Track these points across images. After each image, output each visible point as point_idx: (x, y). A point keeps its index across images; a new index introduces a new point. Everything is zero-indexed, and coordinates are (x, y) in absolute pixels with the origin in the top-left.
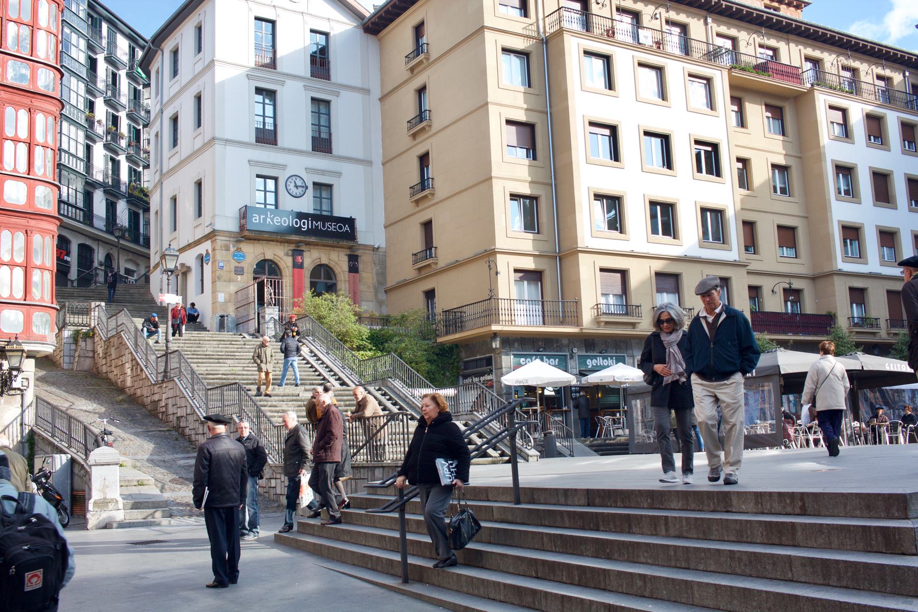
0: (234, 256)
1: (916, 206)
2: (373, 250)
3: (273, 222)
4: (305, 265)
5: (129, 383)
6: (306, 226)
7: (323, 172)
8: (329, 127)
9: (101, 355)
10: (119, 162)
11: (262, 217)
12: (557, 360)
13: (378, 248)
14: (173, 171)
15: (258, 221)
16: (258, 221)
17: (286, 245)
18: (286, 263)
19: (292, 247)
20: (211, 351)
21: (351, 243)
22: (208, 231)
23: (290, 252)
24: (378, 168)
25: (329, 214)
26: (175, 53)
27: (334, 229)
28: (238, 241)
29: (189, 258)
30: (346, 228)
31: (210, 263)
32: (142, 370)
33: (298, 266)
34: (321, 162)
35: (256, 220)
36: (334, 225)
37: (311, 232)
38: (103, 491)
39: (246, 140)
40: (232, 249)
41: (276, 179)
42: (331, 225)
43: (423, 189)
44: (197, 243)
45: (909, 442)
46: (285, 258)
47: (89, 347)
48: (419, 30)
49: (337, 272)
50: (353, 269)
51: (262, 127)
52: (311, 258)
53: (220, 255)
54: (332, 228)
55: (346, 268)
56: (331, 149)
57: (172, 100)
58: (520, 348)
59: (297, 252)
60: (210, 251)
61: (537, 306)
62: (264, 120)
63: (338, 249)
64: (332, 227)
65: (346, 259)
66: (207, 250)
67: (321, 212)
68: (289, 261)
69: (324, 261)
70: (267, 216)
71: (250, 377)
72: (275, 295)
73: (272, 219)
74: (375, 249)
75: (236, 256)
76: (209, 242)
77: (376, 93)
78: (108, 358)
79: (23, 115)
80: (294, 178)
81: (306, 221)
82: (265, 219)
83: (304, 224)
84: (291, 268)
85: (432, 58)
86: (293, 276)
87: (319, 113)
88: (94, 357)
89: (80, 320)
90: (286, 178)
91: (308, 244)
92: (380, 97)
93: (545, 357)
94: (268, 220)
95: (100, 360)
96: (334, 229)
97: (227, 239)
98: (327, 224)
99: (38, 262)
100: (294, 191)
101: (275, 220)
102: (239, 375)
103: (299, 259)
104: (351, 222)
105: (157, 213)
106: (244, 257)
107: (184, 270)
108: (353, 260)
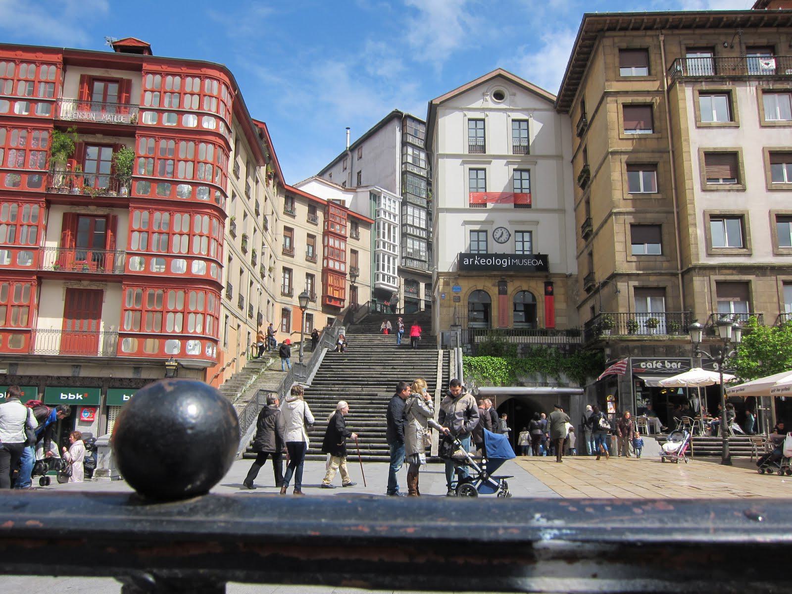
0: (453, 289)
1: (789, 180)
3: (480, 263)
12: (680, 364)
17: (494, 278)
18: (494, 291)
19: (499, 279)
21: (544, 274)
25: (485, 252)
28: (456, 279)
30: (540, 262)
33: (503, 292)
39: (462, 207)
40: (452, 284)
41: (486, 231)
46: (493, 288)
50: (549, 294)
55: (543, 292)
58: (640, 353)
61: (661, 318)
63: (537, 278)
65: (543, 285)
67: (523, 253)
68: (496, 290)
70: (475, 259)
73: (479, 261)
79: (412, 209)
80: (503, 230)
82: (473, 262)
83: (504, 262)
84: (497, 295)
86: (499, 301)
89: (16, 342)
90: (494, 230)
91: (511, 276)
93: (666, 362)
100: (497, 235)
103: (550, 288)
104: (544, 258)
108: (548, 284)
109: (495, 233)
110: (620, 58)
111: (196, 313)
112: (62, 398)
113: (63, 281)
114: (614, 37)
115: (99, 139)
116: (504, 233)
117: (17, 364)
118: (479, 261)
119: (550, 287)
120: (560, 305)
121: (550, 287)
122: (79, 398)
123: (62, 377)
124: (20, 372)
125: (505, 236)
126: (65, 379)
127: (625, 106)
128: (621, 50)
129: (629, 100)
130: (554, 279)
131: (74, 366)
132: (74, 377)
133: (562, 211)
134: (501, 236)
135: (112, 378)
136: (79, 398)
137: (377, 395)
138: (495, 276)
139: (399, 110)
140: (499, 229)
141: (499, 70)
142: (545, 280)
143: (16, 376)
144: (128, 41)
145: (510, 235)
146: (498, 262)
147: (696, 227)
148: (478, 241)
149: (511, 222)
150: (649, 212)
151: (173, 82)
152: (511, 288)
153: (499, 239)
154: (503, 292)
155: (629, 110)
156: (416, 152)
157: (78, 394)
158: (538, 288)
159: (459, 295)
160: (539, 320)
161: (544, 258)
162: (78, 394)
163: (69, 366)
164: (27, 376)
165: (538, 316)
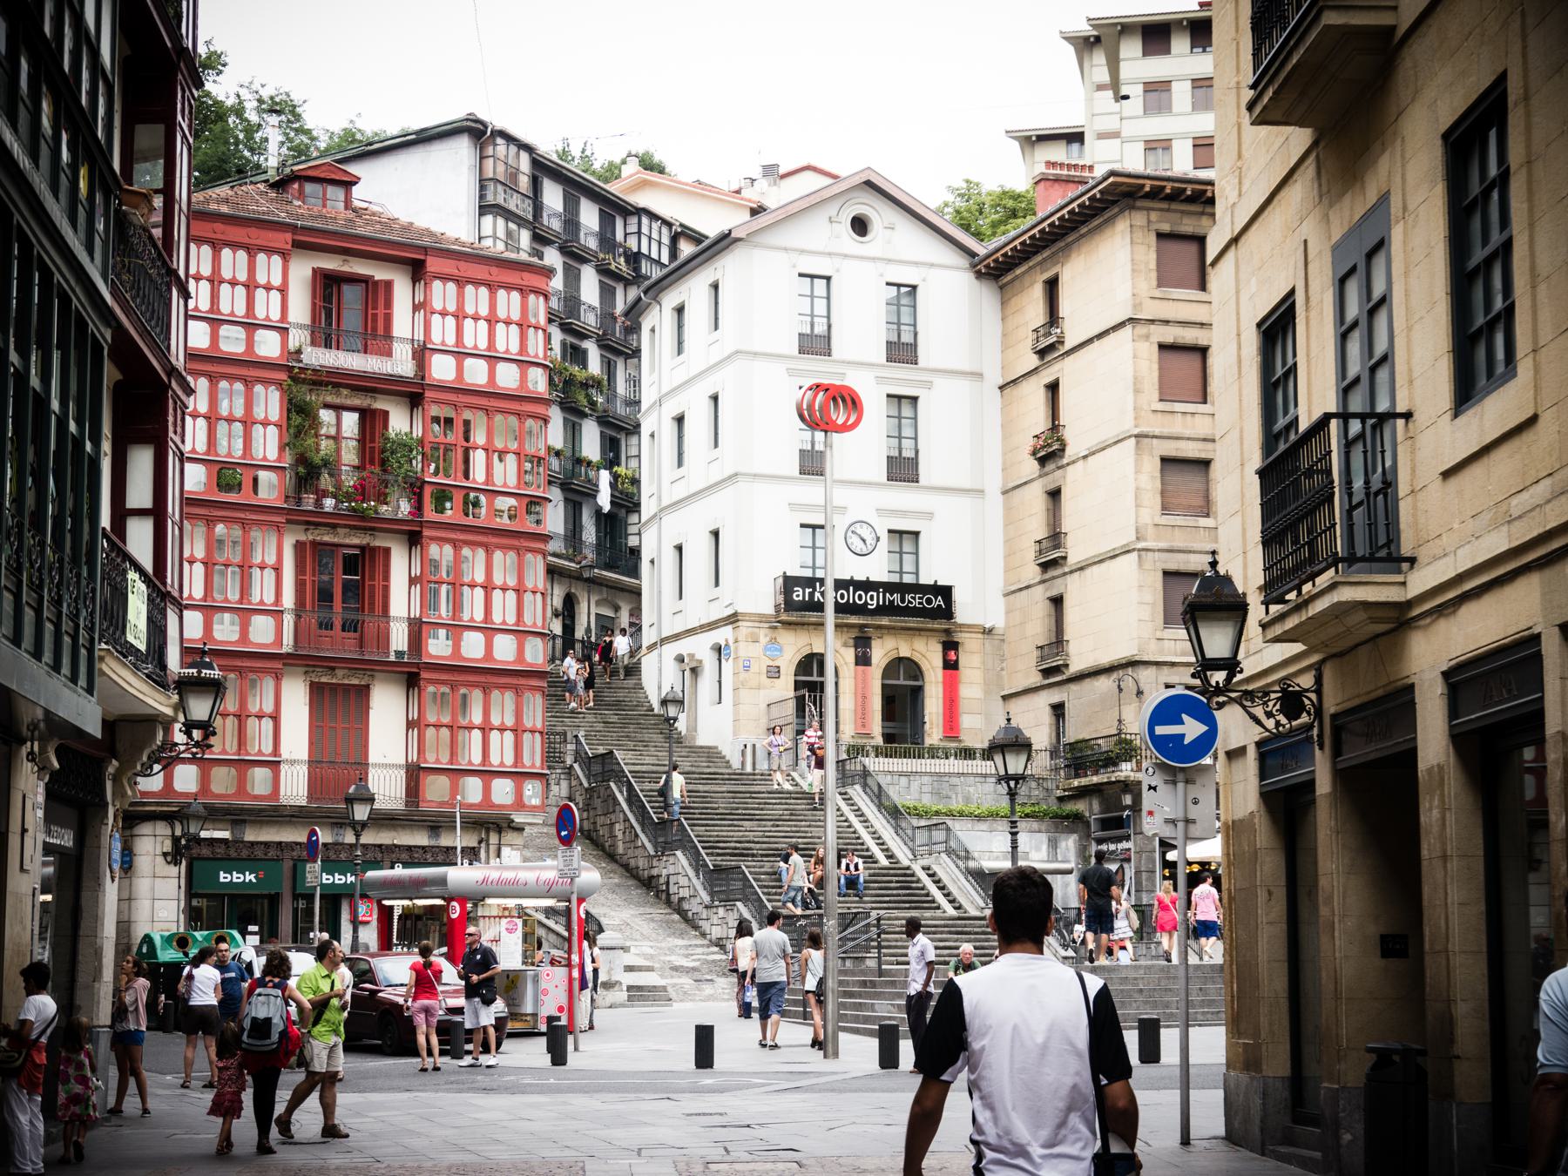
0: (766, 649)
2: (984, 633)
4: (874, 660)
10: (585, 352)
11: (808, 591)
20: (726, 808)
21: (944, 625)
22: (729, 611)
23: (851, 642)
24: (995, 500)
26: (680, 310)
29: (699, 648)
30: (939, 601)
31: (731, 659)
32: (637, 836)
33: (863, 660)
34: (902, 497)
38: (609, 972)
42: (914, 598)
43: (1057, 546)
48: (1052, 285)
49: (924, 668)
50: (951, 666)
51: (809, 448)
53: (746, 650)
54: (916, 603)
60: (731, 642)
64: (915, 601)
65: (939, 648)
70: (815, 590)
74: (988, 632)
75: (770, 649)
78: (592, 813)
82: (812, 595)
97: (757, 624)
98: (908, 597)
99: (528, 724)
100: (858, 545)
102: (758, 843)
104: (946, 592)
105: (652, 435)
106: (781, 650)
108: (950, 646)
110: (1158, 252)
111: (437, 726)
112: (222, 880)
113: (304, 669)
114: (1149, 209)
115: (345, 397)
117: (244, 821)
119: (953, 653)
120: (972, 685)
121: (953, 653)
124: (250, 835)
126: (421, 851)
127: (1163, 347)
128: (1161, 236)
129: (1170, 335)
130: (963, 635)
131: (336, 823)
132: (336, 844)
135: (396, 846)
141: (869, 172)
143: (243, 842)
144: (324, 168)
145: (878, 539)
148: (814, 547)
150: (1194, 552)
151: (476, 298)
152: (881, 652)
154: (863, 660)
155: (1171, 356)
156: (512, 226)
158: (929, 655)
159: (776, 663)
161: (946, 592)
163: (227, 820)
164: (261, 843)
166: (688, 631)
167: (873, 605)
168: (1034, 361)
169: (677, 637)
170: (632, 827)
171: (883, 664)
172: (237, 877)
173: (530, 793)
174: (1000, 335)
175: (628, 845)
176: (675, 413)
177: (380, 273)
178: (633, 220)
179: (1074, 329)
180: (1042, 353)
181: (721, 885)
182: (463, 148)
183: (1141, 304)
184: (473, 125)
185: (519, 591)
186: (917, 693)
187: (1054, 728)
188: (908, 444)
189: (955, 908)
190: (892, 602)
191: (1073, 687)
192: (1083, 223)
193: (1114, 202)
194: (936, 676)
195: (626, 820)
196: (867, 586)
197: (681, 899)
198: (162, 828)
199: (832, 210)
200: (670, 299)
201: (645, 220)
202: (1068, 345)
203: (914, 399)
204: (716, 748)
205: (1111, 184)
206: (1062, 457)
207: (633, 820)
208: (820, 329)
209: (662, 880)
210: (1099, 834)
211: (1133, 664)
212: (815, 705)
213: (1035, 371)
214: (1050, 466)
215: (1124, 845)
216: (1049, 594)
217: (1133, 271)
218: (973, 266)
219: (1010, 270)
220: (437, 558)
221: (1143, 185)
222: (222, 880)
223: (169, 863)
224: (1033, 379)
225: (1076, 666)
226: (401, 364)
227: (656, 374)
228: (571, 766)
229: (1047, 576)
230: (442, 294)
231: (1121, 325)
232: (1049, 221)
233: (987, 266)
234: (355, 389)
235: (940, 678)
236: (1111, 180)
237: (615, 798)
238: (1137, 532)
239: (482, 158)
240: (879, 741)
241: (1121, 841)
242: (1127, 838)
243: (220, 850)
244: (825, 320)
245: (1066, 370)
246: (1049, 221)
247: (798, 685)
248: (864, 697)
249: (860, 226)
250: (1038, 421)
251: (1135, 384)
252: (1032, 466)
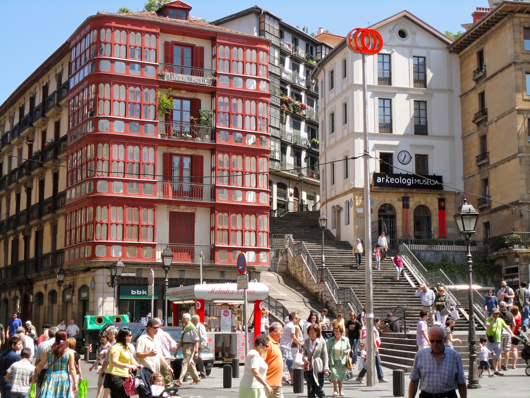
3: (389, 181)
5: (305, 282)
6: (410, 183)
7: (422, 147)
8: (426, 118)
9: (291, 264)
11: (383, 178)
13: (459, 193)
14: (331, 147)
15: (380, 181)
16: (380, 181)
18: (398, 205)
27: (428, 183)
32: (311, 276)
33: (406, 206)
34: (421, 140)
35: (379, 181)
36: (428, 181)
37: (414, 186)
42: (426, 181)
44: (345, 194)
45: (215, 334)
47: (285, 260)
48: (481, 55)
52: (415, 201)
56: (427, 132)
57: (330, 102)
59: (405, 201)
60: (353, 199)
62: (384, 118)
65: (437, 201)
66: (351, 199)
68: (400, 204)
69: (423, 203)
70: (386, 178)
71: (378, 277)
72: (390, 228)
73: (389, 180)
76: (352, 194)
77: (458, 92)
80: (406, 153)
81: (410, 180)
82: (385, 180)
83: (409, 181)
84: (402, 208)
85: (488, 75)
86: (403, 213)
87: (419, 109)
88: (287, 265)
92: (460, 94)
94: (387, 180)
95: (290, 267)
96: (428, 183)
100: (402, 158)
101: (391, 180)
104: (439, 178)
107: (339, 209)
108: (441, 200)
109: (399, 156)
112: (132, 294)
115: (183, 94)
116: (407, 155)
118: (389, 180)
122: (144, 294)
123: (173, 279)
125: (407, 158)
131: (181, 270)
132: (181, 279)
133: (451, 138)
134: (405, 158)
136: (144, 294)
137: (387, 291)
138: (400, 193)
139: (259, 6)
140: (403, 152)
142: (439, 196)
143: (141, 278)
144: (177, 3)
145: (411, 158)
146: (404, 181)
147: (453, 92)
149: (412, 146)
151: (238, 53)
152: (413, 203)
153: (403, 161)
157: (143, 291)
160: (434, 230)
162: (143, 291)
165: (432, 227)
166: (337, 196)
167: (409, 184)
168: (473, 84)
169: (332, 199)
170: (309, 272)
171: (414, 208)
172: (139, 292)
173: (262, 257)
174: (459, 76)
175: (307, 280)
176: (330, 112)
177: (198, 42)
178: (319, 48)
179: (490, 70)
180: (477, 81)
181: (342, 296)
182: (253, 19)
183: (518, 56)
184: (256, 10)
185: (257, 174)
186: (429, 219)
187: (485, 232)
188: (422, 120)
189: (415, 284)
190: (417, 183)
191: (493, 215)
192: (493, 25)
193: (506, 15)
194: (436, 212)
195: (307, 269)
196: (407, 176)
197: (327, 302)
198: (107, 272)
199: (391, 27)
200: (328, 67)
201: (323, 48)
202: (488, 75)
203: (425, 102)
204: (348, 242)
205: (504, 7)
206: (487, 121)
207: (309, 270)
208: (387, 76)
209: (320, 294)
210: (506, 275)
211: (517, 203)
212: (386, 223)
213: (474, 89)
214: (482, 126)
215: (516, 279)
216: (482, 178)
217: (515, 42)
218: (448, 48)
219: (463, 49)
220: (222, 160)
221: (518, 7)
222: (132, 294)
223: (110, 286)
224: (474, 92)
225: (494, 206)
226: (205, 81)
227: (323, 98)
228: (287, 249)
229: (481, 171)
230: (223, 51)
231: (510, 65)
232: (478, 26)
233: (454, 48)
234: (188, 90)
235: (438, 213)
236: (504, 5)
237: (303, 261)
238: (519, 149)
239: (260, 23)
240: (413, 238)
241: (514, 278)
242: (517, 276)
243: (132, 281)
244: (388, 71)
245: (489, 87)
246: (478, 26)
247: (380, 216)
248: (407, 221)
249: (402, 34)
250: (474, 106)
251: (516, 88)
252: (473, 126)
